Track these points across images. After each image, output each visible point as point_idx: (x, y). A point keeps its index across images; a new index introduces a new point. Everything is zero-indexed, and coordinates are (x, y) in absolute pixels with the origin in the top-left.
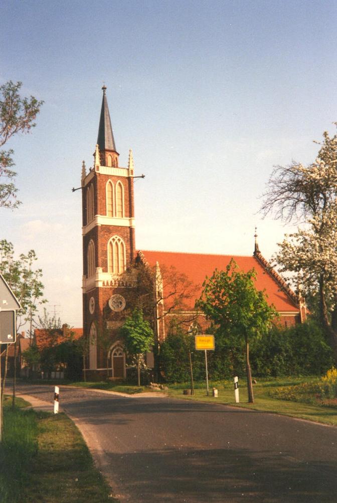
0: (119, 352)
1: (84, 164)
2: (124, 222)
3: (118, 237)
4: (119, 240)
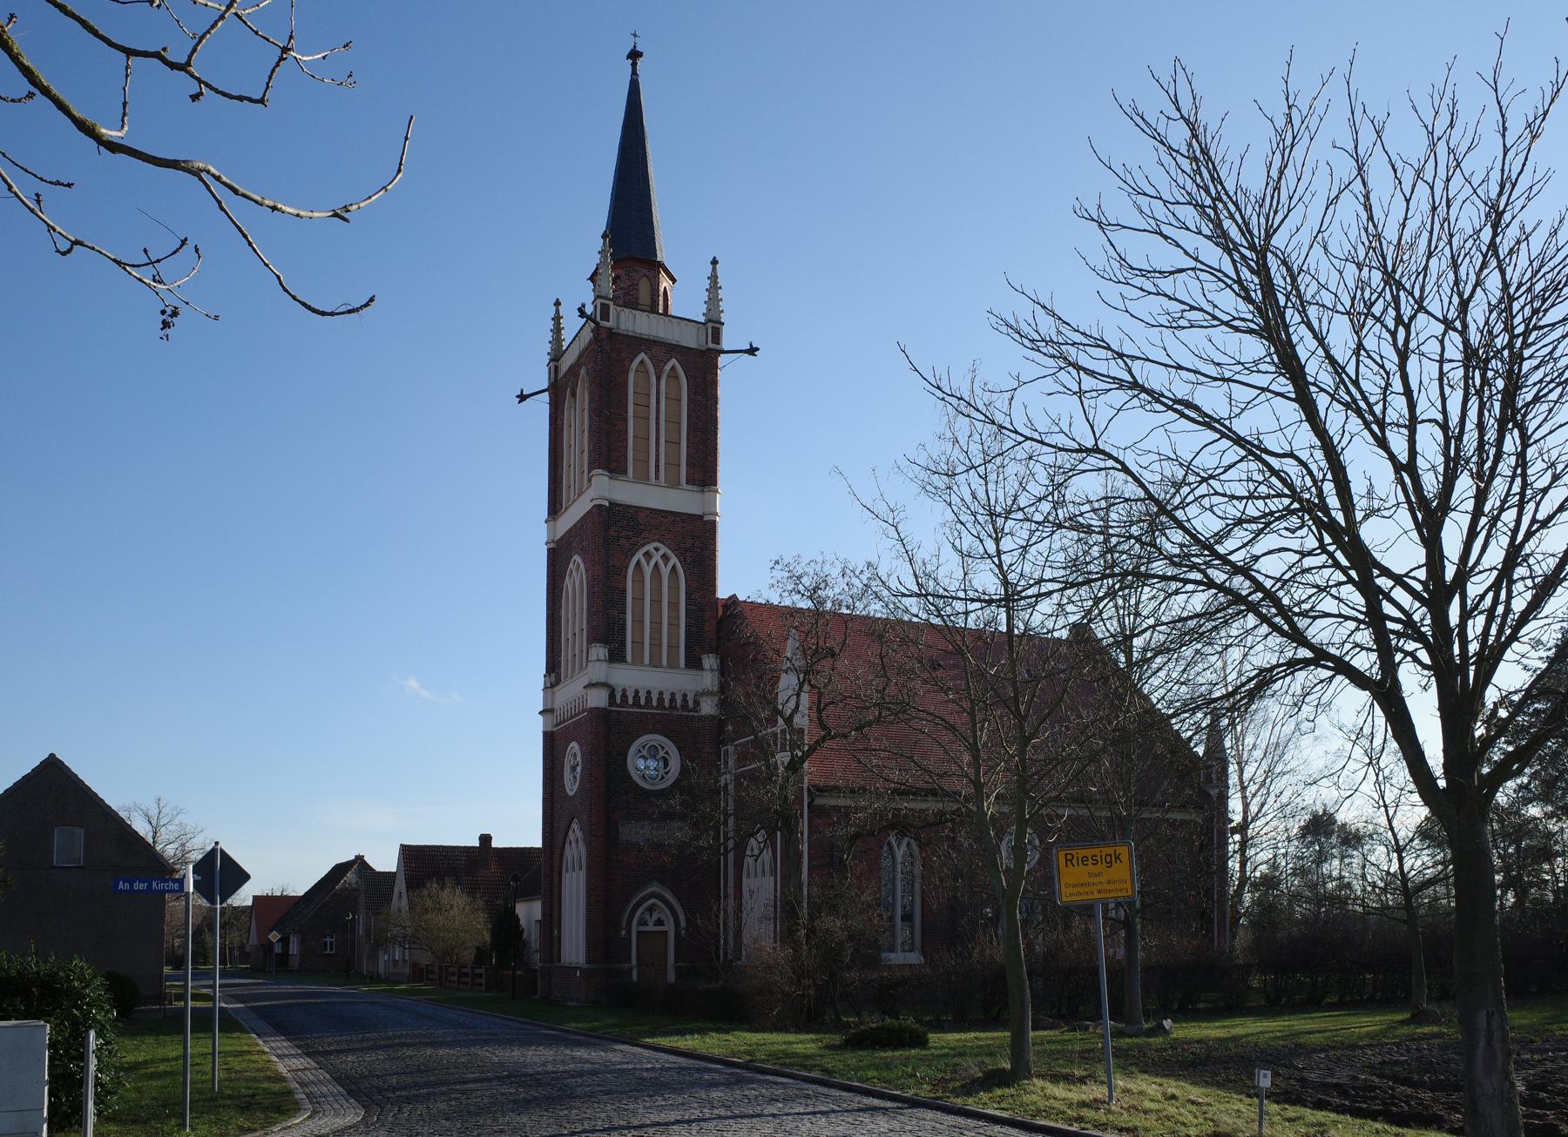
0: (655, 916)
1: (557, 311)
2: (681, 500)
3: (663, 549)
4: (665, 557)
